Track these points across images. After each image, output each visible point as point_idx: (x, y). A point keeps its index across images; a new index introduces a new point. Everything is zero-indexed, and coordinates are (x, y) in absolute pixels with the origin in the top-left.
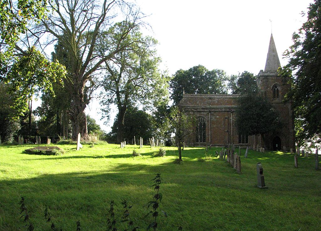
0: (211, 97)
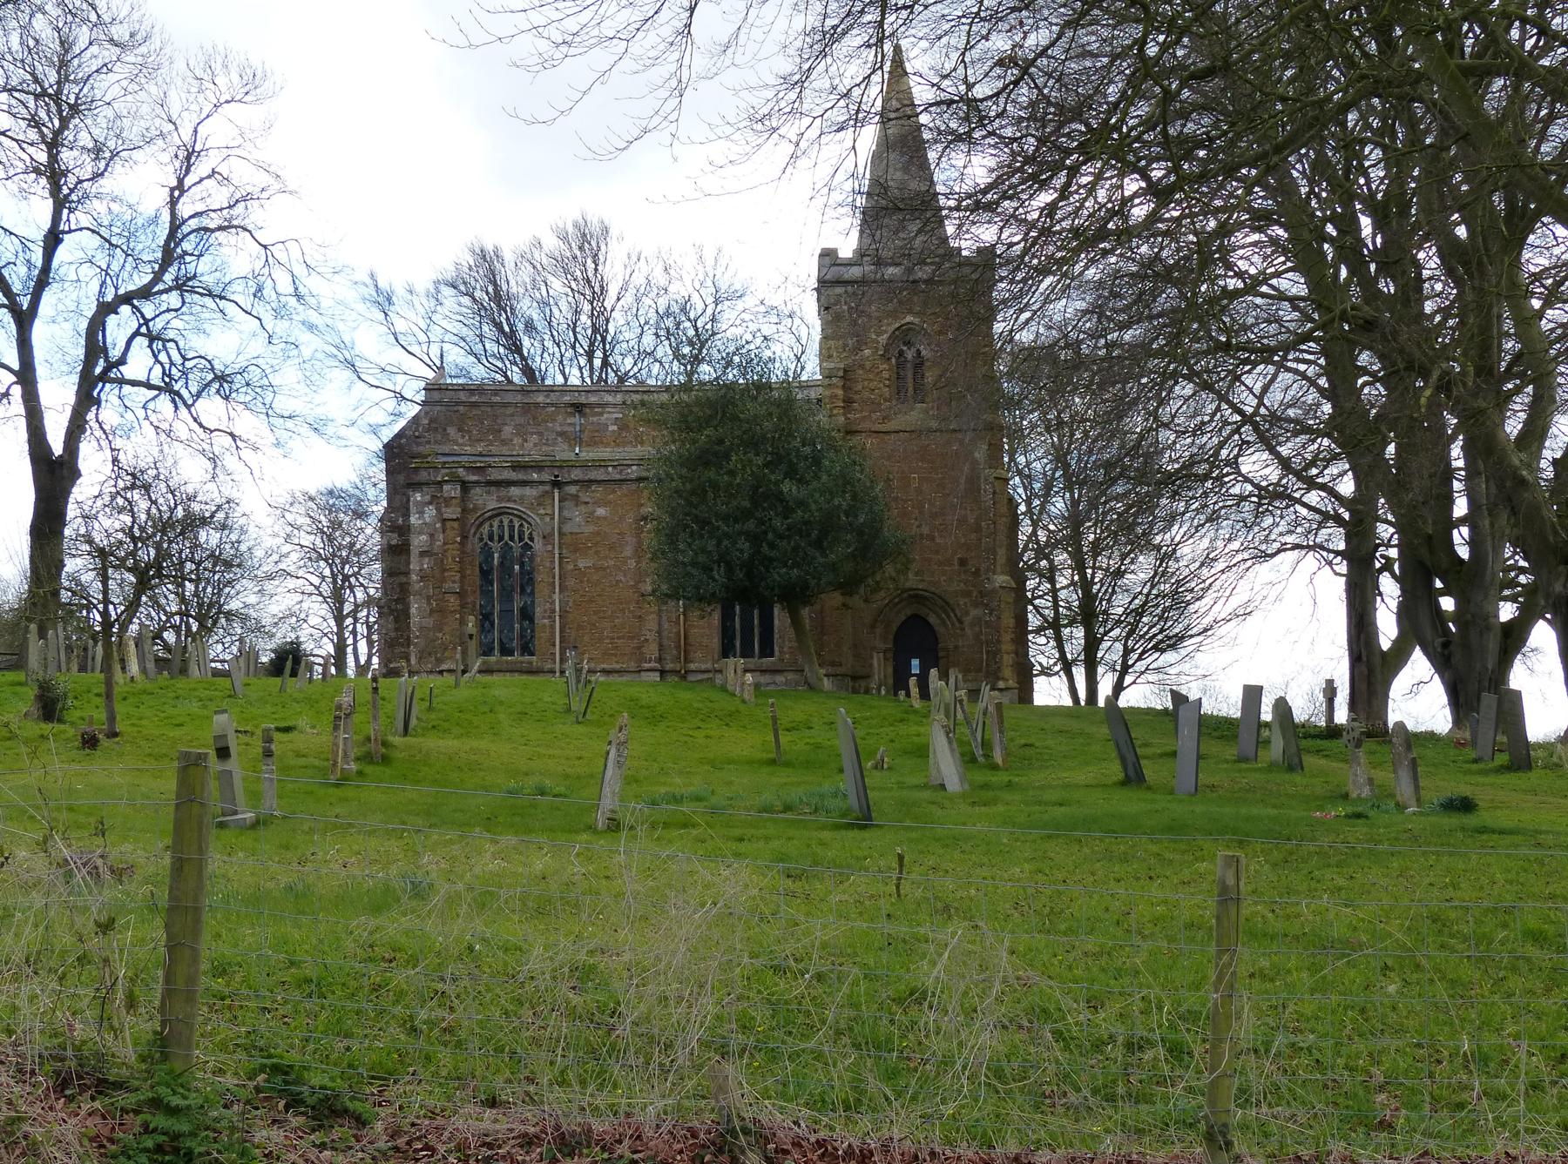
0: (583, 400)
